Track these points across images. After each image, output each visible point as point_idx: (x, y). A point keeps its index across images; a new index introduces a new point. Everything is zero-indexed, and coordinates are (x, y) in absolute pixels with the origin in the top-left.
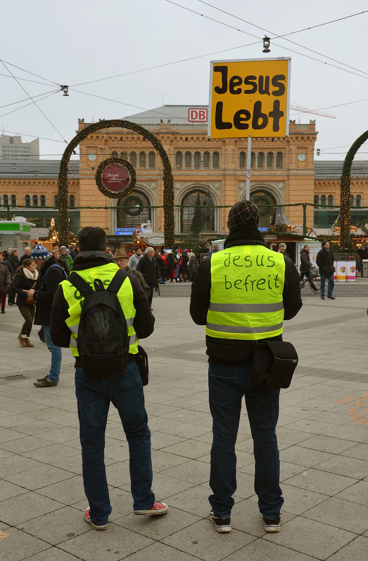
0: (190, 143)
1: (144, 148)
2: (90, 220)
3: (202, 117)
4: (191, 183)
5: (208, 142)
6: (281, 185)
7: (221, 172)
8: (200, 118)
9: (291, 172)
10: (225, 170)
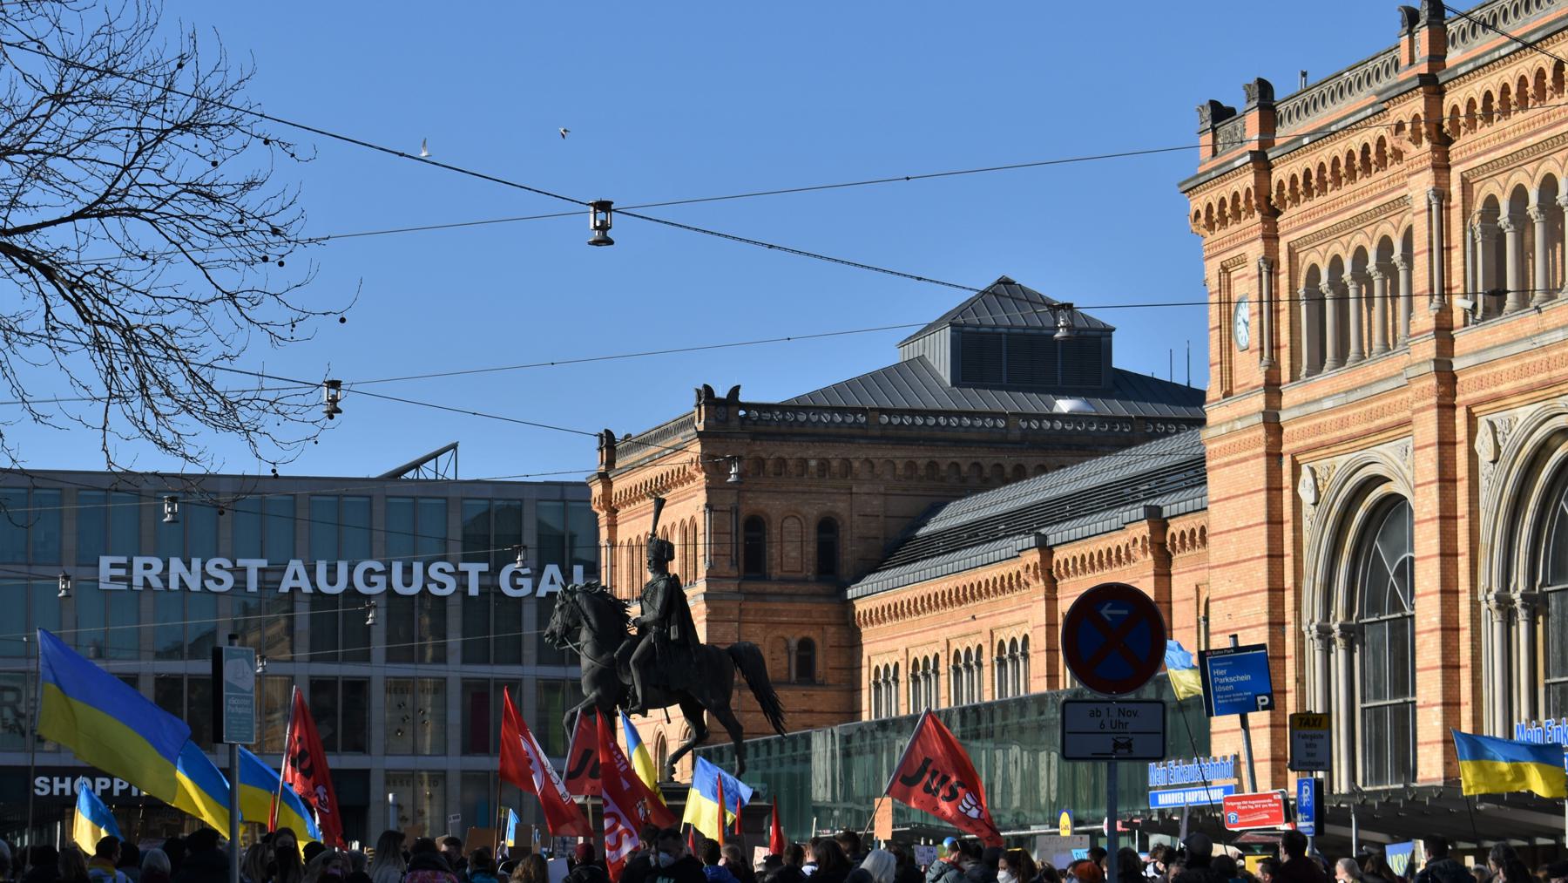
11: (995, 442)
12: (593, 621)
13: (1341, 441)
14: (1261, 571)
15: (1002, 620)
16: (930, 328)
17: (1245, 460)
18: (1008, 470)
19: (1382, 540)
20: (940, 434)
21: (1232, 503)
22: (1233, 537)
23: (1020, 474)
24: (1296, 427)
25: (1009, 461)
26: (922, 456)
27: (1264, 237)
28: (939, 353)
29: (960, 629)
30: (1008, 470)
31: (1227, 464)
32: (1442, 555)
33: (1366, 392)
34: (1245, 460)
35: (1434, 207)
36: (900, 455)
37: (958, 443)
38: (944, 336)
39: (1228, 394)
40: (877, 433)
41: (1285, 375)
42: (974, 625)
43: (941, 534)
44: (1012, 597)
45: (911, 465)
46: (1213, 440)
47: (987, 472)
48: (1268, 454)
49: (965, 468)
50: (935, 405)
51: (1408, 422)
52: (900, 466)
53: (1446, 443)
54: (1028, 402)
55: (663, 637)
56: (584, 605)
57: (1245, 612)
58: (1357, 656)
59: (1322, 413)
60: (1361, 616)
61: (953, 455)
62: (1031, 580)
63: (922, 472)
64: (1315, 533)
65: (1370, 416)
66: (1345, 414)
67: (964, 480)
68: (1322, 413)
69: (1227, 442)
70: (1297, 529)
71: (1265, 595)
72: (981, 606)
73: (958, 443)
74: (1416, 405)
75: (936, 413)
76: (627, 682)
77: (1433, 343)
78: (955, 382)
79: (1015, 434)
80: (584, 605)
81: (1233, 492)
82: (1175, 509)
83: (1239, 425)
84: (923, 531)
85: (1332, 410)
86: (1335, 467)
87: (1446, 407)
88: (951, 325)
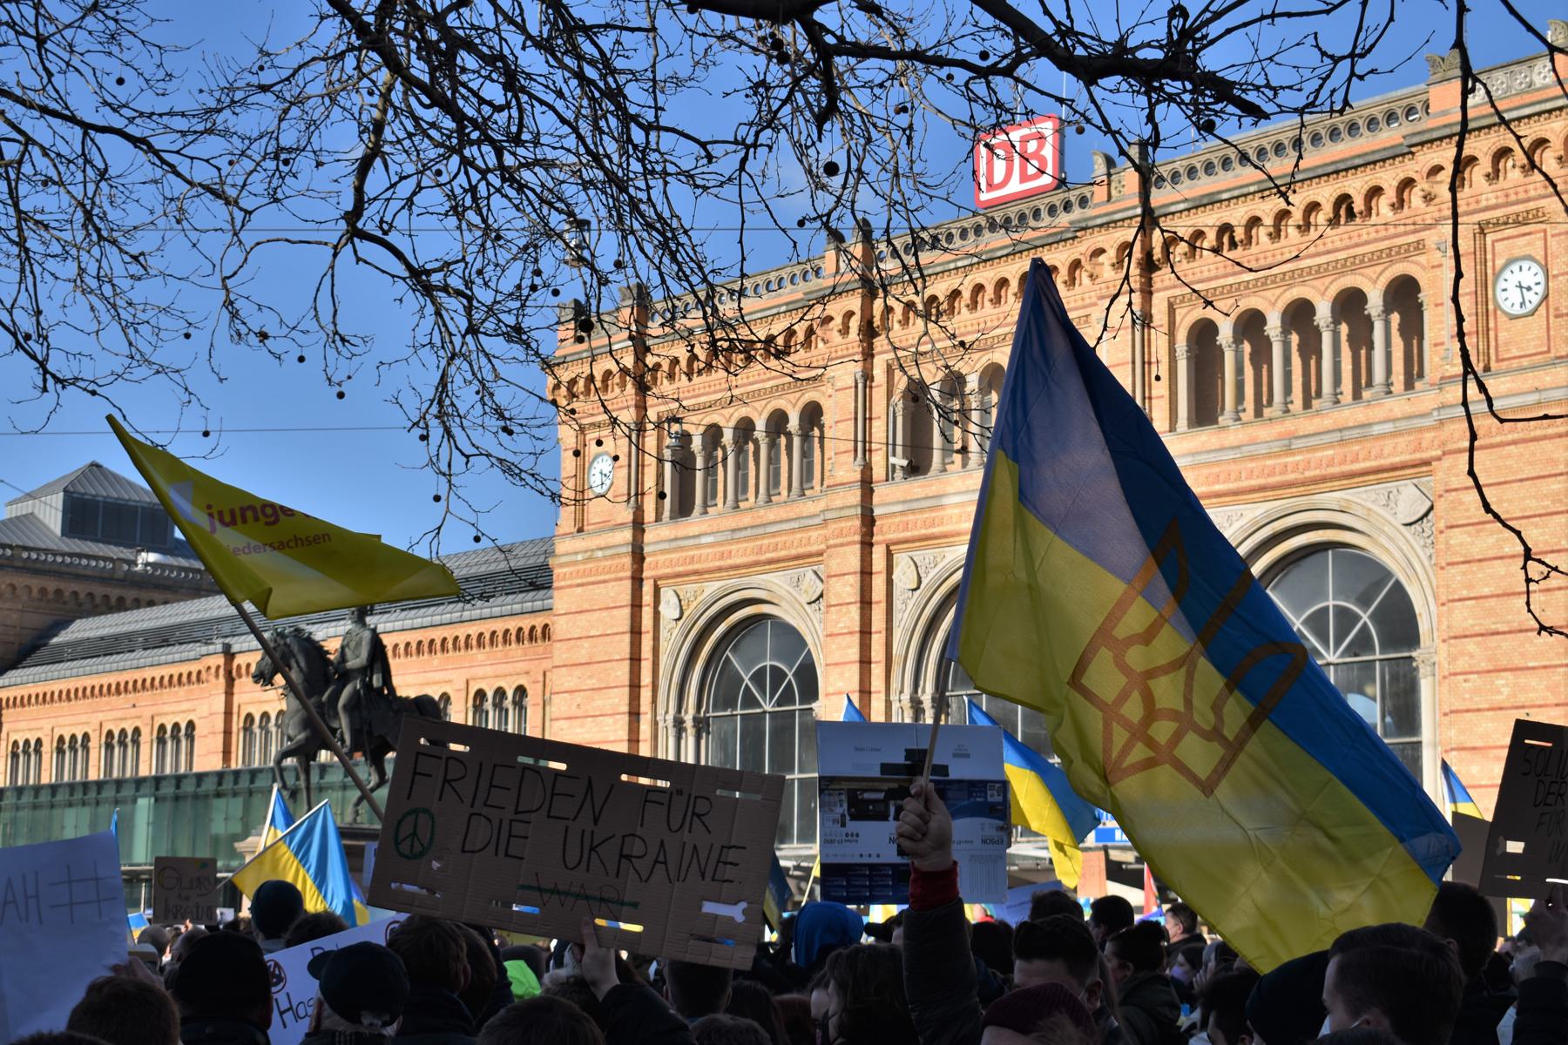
8: (1024, 178)
11: (106, 579)
12: (303, 664)
13: (720, 569)
14: (622, 672)
15: (166, 708)
16: (47, 489)
17: (605, 581)
18: (113, 600)
19: (734, 650)
20: (64, 569)
21: (583, 616)
22: (586, 643)
23: (121, 606)
24: (661, 558)
25: (130, 594)
26: (52, 585)
27: (637, 406)
28: (51, 515)
29: (119, 714)
30: (113, 600)
31: (582, 585)
32: (861, 662)
33: (761, 531)
34: (605, 581)
35: (860, 386)
36: (36, 583)
37: (78, 577)
38: (58, 500)
39: (580, 530)
40: (19, 564)
41: (650, 514)
42: (133, 712)
43: (74, 644)
44: (181, 692)
45: (43, 591)
46: (561, 565)
47: (98, 600)
48: (633, 578)
49: (82, 596)
50: (53, 547)
51: (821, 554)
52: (35, 591)
53: (866, 573)
54: (126, 553)
55: (368, 686)
56: (295, 649)
57: (599, 703)
58: (703, 742)
59: (699, 546)
60: (707, 711)
61: (75, 586)
62: (212, 678)
63: (51, 596)
64: (673, 641)
65: (760, 551)
66: (728, 548)
67: (80, 605)
68: (699, 546)
69: (581, 567)
70: (656, 638)
71: (627, 690)
72: (144, 698)
73: (78, 577)
74: (831, 542)
75: (47, 551)
76: (335, 725)
77: (858, 492)
78: (63, 534)
79: (120, 575)
80: (295, 649)
81: (586, 606)
82: (389, 626)
83: (600, 554)
84: (55, 640)
85: (712, 545)
86: (706, 593)
87: (867, 545)
88: (65, 491)
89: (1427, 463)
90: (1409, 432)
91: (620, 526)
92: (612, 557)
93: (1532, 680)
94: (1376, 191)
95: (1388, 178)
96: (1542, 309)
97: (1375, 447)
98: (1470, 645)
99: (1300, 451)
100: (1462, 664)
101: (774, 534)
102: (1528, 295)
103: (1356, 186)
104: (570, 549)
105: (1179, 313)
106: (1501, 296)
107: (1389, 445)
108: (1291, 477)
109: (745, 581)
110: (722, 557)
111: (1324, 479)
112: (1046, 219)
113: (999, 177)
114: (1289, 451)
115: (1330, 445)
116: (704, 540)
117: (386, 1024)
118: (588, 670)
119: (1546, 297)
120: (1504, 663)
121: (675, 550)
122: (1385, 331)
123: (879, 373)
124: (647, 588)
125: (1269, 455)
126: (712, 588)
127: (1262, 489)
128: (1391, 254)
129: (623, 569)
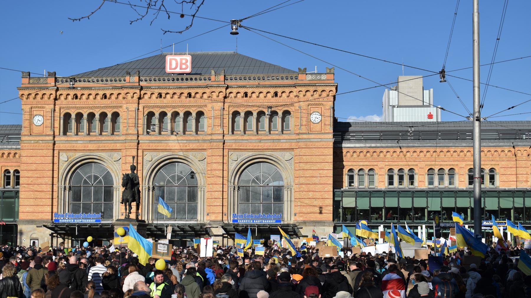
0: (266, 100)
1: (154, 107)
2: (32, 202)
3: (184, 66)
4: (250, 154)
5: (104, 100)
6: (288, 155)
7: (294, 137)
8: (181, 68)
9: (301, 136)
10: (298, 134)
13: (84, 150)
22: (35, 165)
64: (63, 167)
85: (82, 144)
89: (293, 149)
90: (289, 142)
91: (49, 135)
92: (45, 143)
93: (317, 194)
94: (112, 94)
95: (200, 91)
96: (42, 126)
97: (281, 144)
98: (304, 186)
99: (263, 143)
100: (301, 189)
101: (104, 143)
102: (316, 119)
103: (163, 92)
104: (28, 139)
105: (62, 110)
106: (34, 121)
107: (284, 144)
108: (260, 148)
109: (92, 154)
110: (85, 147)
111: (268, 149)
112: (109, 82)
113: (174, 66)
114: (260, 142)
115: (270, 143)
116: (79, 142)
117: (259, 262)
118: (36, 172)
119: (321, 120)
120: (311, 190)
121: (68, 143)
122: (97, 123)
123: (141, 108)
124: (56, 152)
125: (255, 143)
126: (78, 154)
127: (252, 149)
128: (91, 108)
129: (49, 146)
